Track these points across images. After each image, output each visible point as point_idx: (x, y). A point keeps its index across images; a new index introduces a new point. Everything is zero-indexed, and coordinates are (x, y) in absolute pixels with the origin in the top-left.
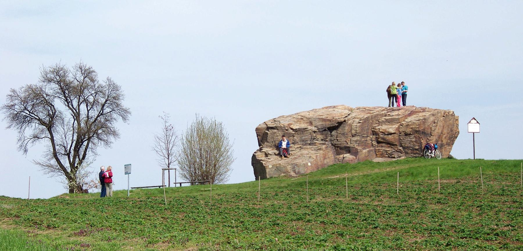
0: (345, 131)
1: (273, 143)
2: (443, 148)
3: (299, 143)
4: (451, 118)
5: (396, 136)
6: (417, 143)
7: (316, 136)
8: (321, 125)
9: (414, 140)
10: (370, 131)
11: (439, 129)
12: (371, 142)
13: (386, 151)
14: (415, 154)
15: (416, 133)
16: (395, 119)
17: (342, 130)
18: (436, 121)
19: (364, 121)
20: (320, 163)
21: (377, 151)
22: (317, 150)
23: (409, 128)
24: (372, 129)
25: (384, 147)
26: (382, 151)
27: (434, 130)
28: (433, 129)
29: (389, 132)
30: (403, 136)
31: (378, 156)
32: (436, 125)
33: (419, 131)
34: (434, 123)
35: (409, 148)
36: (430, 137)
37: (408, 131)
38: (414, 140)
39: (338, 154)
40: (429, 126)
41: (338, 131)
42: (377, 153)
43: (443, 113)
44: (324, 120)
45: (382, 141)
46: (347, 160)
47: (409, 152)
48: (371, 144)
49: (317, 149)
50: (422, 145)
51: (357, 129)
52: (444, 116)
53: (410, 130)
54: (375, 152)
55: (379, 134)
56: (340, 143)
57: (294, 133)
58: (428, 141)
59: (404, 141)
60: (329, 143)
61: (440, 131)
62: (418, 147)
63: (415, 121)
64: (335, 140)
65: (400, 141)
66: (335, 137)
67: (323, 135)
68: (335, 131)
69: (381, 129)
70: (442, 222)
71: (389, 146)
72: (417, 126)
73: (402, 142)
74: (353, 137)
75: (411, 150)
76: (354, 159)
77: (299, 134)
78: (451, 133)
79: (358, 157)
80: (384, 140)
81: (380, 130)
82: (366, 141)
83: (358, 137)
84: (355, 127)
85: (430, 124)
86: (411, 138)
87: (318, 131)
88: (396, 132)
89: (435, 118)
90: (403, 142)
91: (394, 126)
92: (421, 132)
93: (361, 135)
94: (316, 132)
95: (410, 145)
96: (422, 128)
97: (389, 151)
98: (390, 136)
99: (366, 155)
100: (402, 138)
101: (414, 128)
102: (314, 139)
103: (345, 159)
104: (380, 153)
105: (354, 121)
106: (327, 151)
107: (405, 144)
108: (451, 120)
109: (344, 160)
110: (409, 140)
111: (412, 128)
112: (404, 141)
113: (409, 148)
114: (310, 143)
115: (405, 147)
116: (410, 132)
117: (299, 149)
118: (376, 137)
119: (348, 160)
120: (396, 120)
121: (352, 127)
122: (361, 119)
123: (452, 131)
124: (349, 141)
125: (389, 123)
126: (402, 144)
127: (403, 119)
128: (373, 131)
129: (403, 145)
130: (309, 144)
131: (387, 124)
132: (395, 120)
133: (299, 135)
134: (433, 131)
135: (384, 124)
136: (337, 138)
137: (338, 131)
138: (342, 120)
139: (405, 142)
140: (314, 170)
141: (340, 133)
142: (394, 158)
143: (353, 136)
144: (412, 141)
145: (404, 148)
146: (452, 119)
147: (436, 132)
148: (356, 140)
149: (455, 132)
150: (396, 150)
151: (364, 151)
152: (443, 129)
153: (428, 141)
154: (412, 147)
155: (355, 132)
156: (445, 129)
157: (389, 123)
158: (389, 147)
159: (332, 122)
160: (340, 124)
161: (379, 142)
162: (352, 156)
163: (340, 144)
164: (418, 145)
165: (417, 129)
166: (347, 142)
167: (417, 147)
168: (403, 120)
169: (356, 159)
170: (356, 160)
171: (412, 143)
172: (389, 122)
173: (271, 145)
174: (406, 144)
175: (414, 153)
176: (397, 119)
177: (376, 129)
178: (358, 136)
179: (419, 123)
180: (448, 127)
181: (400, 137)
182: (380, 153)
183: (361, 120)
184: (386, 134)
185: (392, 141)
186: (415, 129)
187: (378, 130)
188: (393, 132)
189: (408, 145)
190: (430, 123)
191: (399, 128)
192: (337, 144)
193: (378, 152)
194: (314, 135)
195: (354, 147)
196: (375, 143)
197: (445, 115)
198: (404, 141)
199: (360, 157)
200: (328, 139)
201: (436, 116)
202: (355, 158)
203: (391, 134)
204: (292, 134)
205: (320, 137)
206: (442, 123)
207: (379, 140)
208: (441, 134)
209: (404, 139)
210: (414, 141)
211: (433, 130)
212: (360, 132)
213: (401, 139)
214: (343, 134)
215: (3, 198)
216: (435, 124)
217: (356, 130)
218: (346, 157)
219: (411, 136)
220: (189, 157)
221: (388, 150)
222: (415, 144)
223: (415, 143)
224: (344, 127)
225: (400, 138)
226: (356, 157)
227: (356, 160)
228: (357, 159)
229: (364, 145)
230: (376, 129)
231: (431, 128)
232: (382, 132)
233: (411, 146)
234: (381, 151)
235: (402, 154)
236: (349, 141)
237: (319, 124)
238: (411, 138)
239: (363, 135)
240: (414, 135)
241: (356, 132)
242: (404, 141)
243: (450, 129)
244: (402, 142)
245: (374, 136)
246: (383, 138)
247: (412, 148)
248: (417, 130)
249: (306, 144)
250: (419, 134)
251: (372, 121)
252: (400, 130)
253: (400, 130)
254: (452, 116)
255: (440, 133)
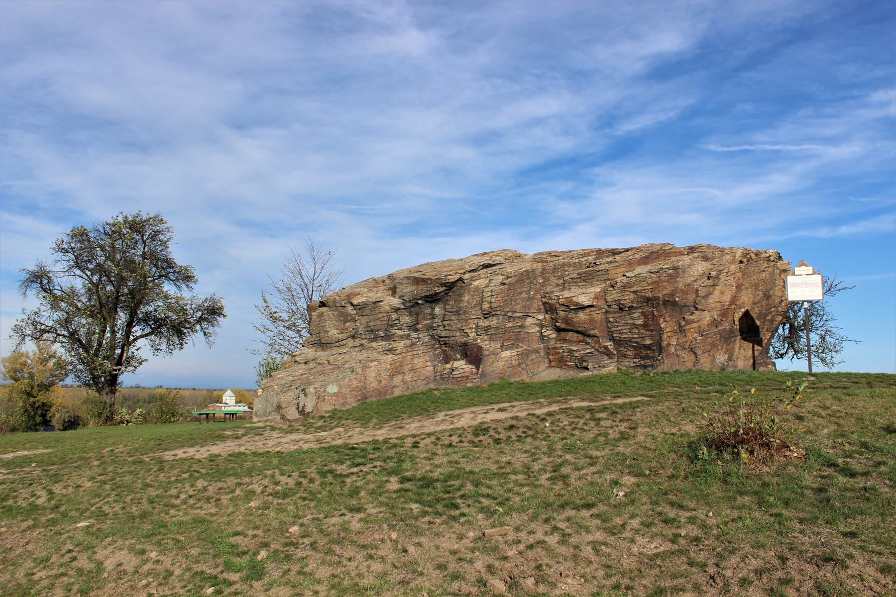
0: (462, 305)
1: (317, 337)
2: (735, 340)
3: (363, 337)
4: (765, 265)
5: (598, 316)
6: (647, 330)
7: (397, 319)
8: (409, 292)
9: (642, 323)
10: (537, 304)
11: (722, 293)
12: (538, 329)
13: (571, 352)
14: (643, 358)
15: (645, 304)
16: (599, 271)
17: (455, 301)
18: (713, 274)
19: (517, 277)
20: (374, 385)
21: (552, 351)
22: (387, 352)
23: (628, 293)
24: (543, 299)
25: (570, 342)
26: (561, 351)
27: (707, 296)
28: (702, 292)
29: (577, 304)
30: (615, 312)
31: (553, 364)
32: (712, 284)
33: (656, 299)
34: (709, 278)
35: (629, 344)
36: (692, 314)
37: (628, 299)
38: (640, 322)
39: (447, 360)
40: (689, 285)
41: (447, 307)
42: (551, 357)
43: (739, 253)
44: (417, 281)
45: (563, 326)
46: (457, 376)
47: (629, 353)
48: (538, 334)
49: (386, 349)
50: (663, 334)
51: (493, 300)
52: (741, 262)
53: (632, 296)
54: (548, 354)
55: (556, 310)
56: (448, 335)
57: (355, 312)
58: (683, 323)
59: (616, 324)
60: (425, 337)
61: (727, 298)
62: (651, 339)
63: (649, 274)
64: (439, 326)
65: (609, 325)
66: (440, 321)
67: (411, 316)
68: (441, 305)
69: (561, 297)
70: (160, 445)
71: (581, 337)
72: (649, 286)
73: (613, 329)
74: (485, 318)
75: (635, 347)
76: (472, 373)
77: (364, 314)
78: (764, 302)
79: (481, 370)
80: (568, 324)
81: (560, 301)
82: (522, 327)
83: (495, 318)
84: (489, 294)
85: (695, 281)
86: (634, 319)
87: (403, 307)
88: (594, 304)
89: (713, 267)
90: (616, 329)
91: (592, 290)
92: (661, 302)
93: (503, 313)
94: (399, 309)
95: (629, 335)
96: (666, 292)
97: (577, 351)
98: (582, 315)
99: (513, 362)
100: (612, 317)
101: (641, 291)
102: (393, 326)
103: (454, 373)
104: (557, 356)
105: (490, 280)
106: (410, 354)
107: (620, 333)
108: (764, 271)
109: (451, 376)
110: (630, 321)
111: (635, 292)
112: (616, 324)
113: (629, 344)
114: (383, 335)
115: (620, 341)
116: (632, 302)
117: (357, 349)
118: (552, 318)
119: (460, 375)
120: (601, 273)
121: (483, 295)
122: (510, 275)
123: (767, 296)
124: (471, 328)
125: (585, 283)
126: (612, 332)
127: (622, 270)
128: (544, 304)
129: (615, 335)
130: (382, 337)
131: (580, 284)
132: (598, 273)
133: (365, 317)
134: (703, 298)
135: (574, 284)
136: (444, 322)
137: (447, 307)
138: (453, 278)
139: (619, 328)
140: (344, 404)
141: (451, 310)
142: (587, 368)
143: (486, 315)
144: (636, 326)
145: (618, 343)
146: (770, 269)
147: (711, 301)
148: (487, 327)
149: (777, 300)
150: (597, 348)
151: (507, 353)
152: (736, 293)
153: (683, 323)
154: (636, 340)
155: (489, 306)
156: (743, 292)
157: (587, 282)
158: (580, 341)
159: (430, 284)
160: (450, 287)
161: (559, 330)
162: (470, 366)
163: (449, 337)
164: (651, 336)
165: (649, 295)
166: (465, 331)
167: (648, 342)
168: (622, 274)
169: (477, 373)
170: (475, 377)
171: (637, 331)
172: (584, 281)
173: (315, 340)
174: (623, 333)
175: (641, 357)
176: (602, 270)
177: (552, 299)
178: (493, 315)
179: (655, 279)
180: (756, 289)
181: (609, 316)
182: (557, 356)
183: (508, 278)
184: (572, 309)
185: (586, 326)
186: (643, 294)
187: (554, 301)
188: (587, 303)
189: (627, 336)
190: (694, 279)
191: (605, 291)
192: (443, 335)
193: (553, 355)
194: (394, 316)
195: (474, 343)
196: (550, 333)
197: (745, 260)
198: (617, 327)
199: (489, 369)
200: (419, 326)
201: (715, 262)
202: (474, 371)
203: (583, 308)
204: (351, 315)
205: (406, 320)
206: (734, 278)
207: (558, 324)
208: (730, 305)
209: (618, 320)
210: (640, 325)
211: (703, 295)
212: (500, 306)
213: (611, 320)
214: (457, 313)
215: (885, 83)
216: (711, 281)
217: (491, 303)
218: (457, 368)
219: (634, 311)
220: (738, 382)
221: (575, 348)
222: (643, 334)
223: (642, 331)
224: (461, 295)
225: (607, 318)
226: (478, 369)
227: (475, 377)
228: (480, 373)
229: (513, 337)
230: (552, 299)
231: (697, 291)
232: (563, 305)
233: (635, 338)
234: (559, 353)
235: (610, 358)
236: (471, 328)
237: (408, 290)
238: (634, 319)
239: (509, 314)
240: (640, 311)
241: (491, 307)
242: (617, 327)
243: (761, 293)
244: (613, 329)
245: (547, 316)
246: (566, 321)
247: (636, 342)
248: (647, 295)
249: (375, 339)
250: (654, 308)
251: (544, 279)
252: (608, 298)
253: (608, 298)
254: (769, 260)
255: (728, 303)
